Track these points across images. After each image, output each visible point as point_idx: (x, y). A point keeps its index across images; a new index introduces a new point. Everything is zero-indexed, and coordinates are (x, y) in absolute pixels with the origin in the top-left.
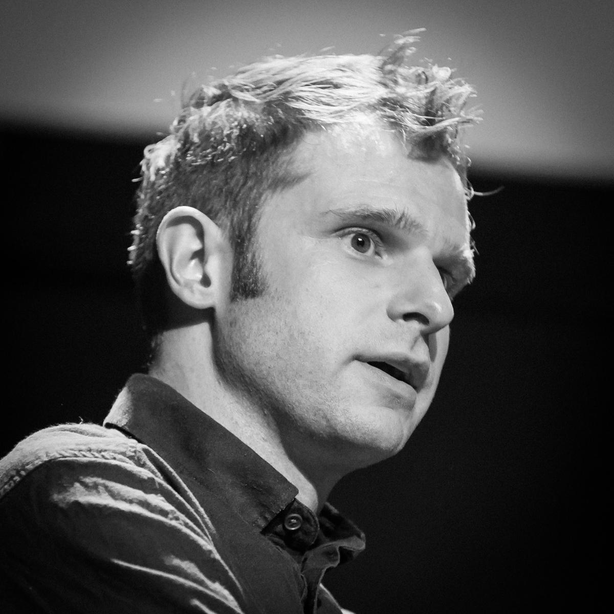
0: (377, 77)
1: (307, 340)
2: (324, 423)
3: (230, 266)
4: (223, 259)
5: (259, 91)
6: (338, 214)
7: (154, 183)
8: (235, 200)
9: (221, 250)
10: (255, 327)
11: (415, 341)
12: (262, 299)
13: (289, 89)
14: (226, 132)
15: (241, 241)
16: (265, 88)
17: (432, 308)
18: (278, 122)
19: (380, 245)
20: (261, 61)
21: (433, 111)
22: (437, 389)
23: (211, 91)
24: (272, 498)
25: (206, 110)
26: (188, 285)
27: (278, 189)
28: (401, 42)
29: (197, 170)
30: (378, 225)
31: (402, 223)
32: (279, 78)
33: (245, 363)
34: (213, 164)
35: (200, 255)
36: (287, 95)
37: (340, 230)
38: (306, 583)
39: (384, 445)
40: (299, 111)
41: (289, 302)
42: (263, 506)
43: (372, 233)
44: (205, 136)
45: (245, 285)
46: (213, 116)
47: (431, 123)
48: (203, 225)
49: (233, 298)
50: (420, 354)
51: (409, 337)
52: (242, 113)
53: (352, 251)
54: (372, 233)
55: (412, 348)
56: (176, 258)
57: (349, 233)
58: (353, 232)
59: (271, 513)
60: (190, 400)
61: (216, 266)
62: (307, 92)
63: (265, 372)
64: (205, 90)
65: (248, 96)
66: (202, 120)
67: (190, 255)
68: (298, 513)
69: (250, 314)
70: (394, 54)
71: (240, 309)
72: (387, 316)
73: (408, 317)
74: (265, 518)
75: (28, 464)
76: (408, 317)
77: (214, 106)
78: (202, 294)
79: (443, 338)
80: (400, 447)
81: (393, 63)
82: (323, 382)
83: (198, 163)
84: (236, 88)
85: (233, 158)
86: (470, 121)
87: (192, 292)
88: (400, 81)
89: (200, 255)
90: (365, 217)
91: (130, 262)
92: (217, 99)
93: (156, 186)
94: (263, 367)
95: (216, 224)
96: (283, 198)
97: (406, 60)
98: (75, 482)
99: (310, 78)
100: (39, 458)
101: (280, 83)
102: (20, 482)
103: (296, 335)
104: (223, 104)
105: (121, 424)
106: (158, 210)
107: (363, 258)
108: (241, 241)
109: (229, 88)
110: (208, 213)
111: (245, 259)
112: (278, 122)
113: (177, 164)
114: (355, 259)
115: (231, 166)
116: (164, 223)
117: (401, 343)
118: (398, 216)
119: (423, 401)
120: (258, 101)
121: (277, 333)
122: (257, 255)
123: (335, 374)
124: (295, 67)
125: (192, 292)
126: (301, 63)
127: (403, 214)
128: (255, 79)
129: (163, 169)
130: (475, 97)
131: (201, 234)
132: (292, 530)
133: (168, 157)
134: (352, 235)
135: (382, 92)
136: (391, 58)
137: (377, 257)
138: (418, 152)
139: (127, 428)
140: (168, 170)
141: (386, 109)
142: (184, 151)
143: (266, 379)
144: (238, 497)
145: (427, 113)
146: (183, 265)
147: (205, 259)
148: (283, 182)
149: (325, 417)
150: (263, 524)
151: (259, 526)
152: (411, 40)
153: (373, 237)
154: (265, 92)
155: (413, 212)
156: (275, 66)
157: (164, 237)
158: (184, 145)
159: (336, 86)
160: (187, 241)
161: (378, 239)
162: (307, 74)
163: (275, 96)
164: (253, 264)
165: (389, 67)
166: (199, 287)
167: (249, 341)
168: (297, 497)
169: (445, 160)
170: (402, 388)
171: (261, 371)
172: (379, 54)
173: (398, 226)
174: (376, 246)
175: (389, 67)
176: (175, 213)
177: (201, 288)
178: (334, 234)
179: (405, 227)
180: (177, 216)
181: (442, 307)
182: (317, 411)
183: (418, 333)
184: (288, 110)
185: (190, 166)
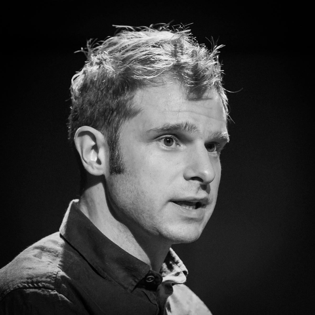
1: (145, 196)
6: (155, 131)
9: (104, 145)
10: (121, 189)
11: (199, 189)
12: (124, 174)
15: (112, 145)
17: (203, 174)
19: (178, 141)
26: (91, 164)
27: (126, 118)
30: (174, 132)
31: (187, 128)
35: (95, 148)
37: (157, 138)
38: (158, 308)
41: (136, 177)
42: (135, 276)
43: (173, 136)
45: (116, 167)
48: (95, 135)
49: (111, 173)
50: (202, 195)
51: (195, 188)
54: (173, 136)
55: (197, 192)
56: (84, 150)
57: (162, 139)
58: (163, 138)
59: (138, 279)
60: (96, 226)
68: (152, 275)
72: (183, 178)
73: (194, 178)
74: (135, 281)
76: (194, 178)
78: (98, 168)
87: (93, 168)
90: (168, 130)
96: (129, 123)
103: (140, 193)
107: (170, 149)
108: (112, 145)
114: (166, 151)
116: (77, 133)
117: (192, 191)
118: (184, 125)
119: (208, 211)
121: (131, 192)
123: (160, 211)
127: (186, 124)
130: (220, 53)
131: (94, 138)
132: (151, 282)
134: (163, 139)
137: (178, 146)
138: (192, 95)
143: (129, 213)
146: (88, 152)
149: (158, 231)
150: (135, 284)
151: (133, 285)
155: (191, 121)
160: (89, 142)
161: (177, 139)
164: (118, 155)
167: (120, 195)
171: (126, 209)
173: (185, 130)
174: (176, 141)
176: (79, 130)
177: (97, 165)
178: (155, 140)
179: (189, 130)
180: (79, 132)
183: (199, 186)
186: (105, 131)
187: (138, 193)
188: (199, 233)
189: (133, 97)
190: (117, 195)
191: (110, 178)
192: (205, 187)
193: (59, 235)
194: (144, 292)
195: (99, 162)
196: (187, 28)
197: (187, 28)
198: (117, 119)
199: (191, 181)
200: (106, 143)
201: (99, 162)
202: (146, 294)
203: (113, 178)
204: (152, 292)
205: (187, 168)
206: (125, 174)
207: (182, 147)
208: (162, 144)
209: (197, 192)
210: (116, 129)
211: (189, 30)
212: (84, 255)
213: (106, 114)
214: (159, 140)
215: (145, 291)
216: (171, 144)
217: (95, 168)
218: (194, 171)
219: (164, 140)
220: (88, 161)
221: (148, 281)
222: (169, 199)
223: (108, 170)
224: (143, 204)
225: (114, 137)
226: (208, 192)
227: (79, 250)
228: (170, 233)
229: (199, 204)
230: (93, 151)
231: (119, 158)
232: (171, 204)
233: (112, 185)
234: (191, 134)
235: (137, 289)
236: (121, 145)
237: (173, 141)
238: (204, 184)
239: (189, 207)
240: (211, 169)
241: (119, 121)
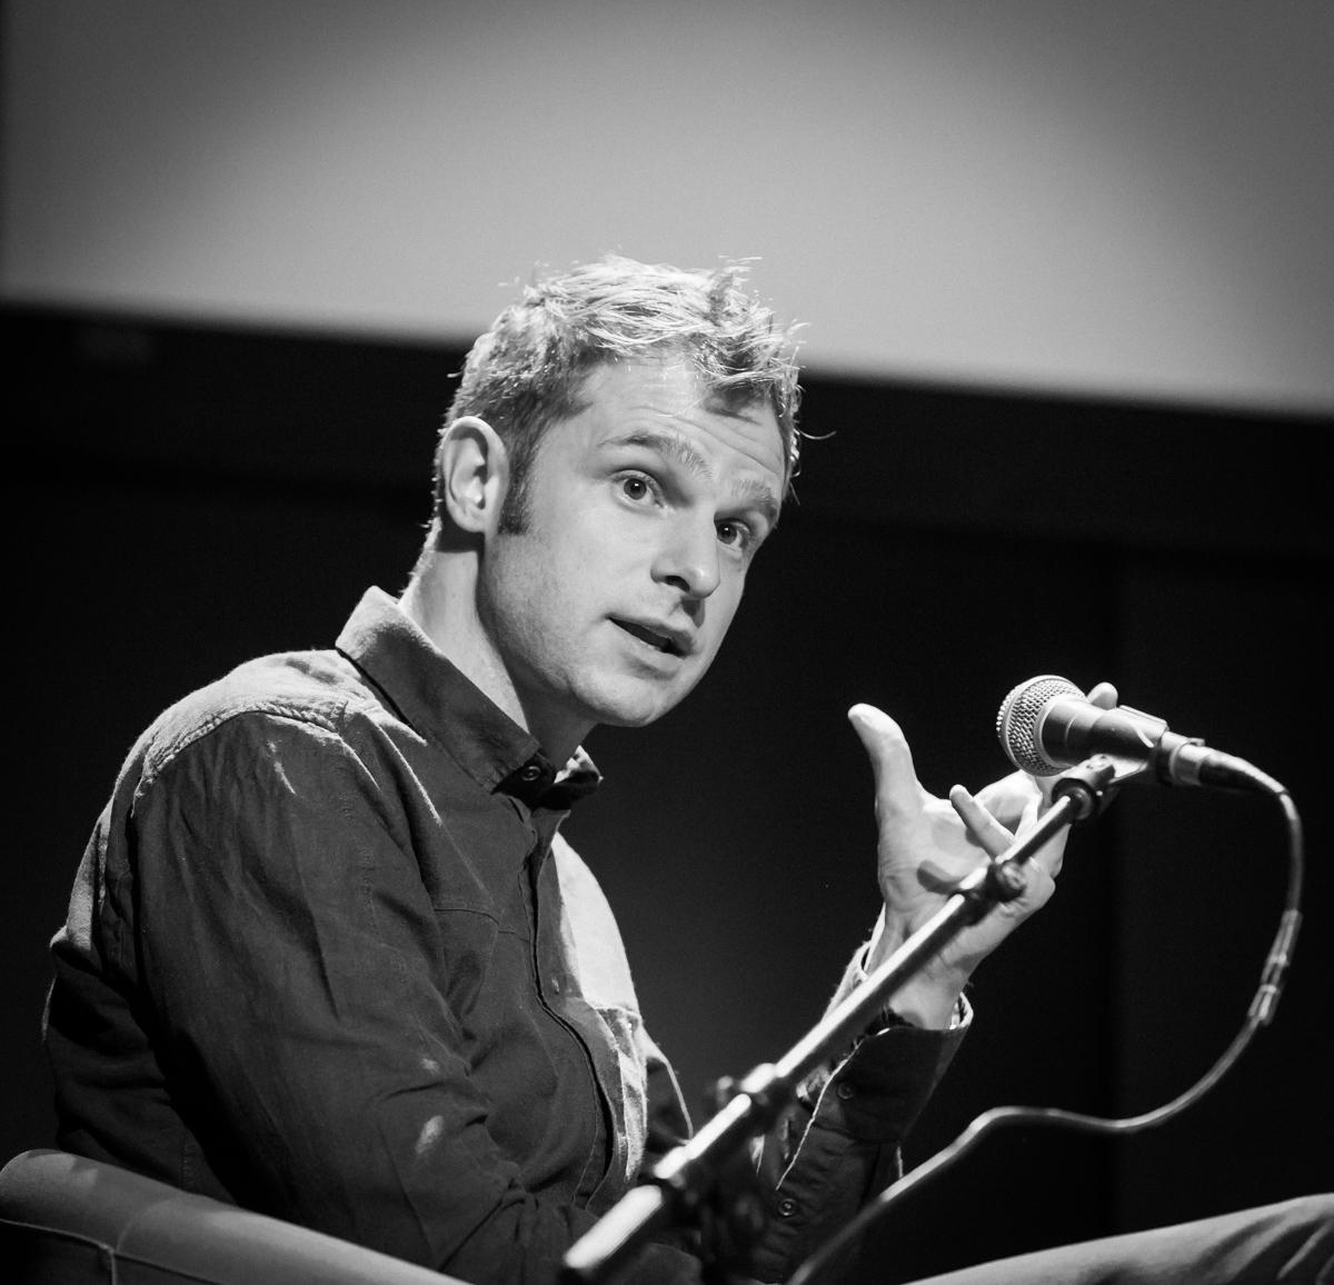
2: (564, 682)
4: (502, 481)
10: (513, 567)
13: (596, 311)
15: (519, 468)
17: (693, 574)
22: (716, 657)
26: (462, 503)
32: (595, 294)
33: (498, 602)
42: (501, 761)
43: (650, 483)
45: (512, 520)
49: (500, 530)
50: (681, 622)
53: (625, 498)
55: (671, 614)
57: (623, 478)
59: (507, 768)
67: (473, 469)
74: (501, 774)
75: (224, 712)
80: (649, 720)
82: (569, 640)
86: (665, 446)
87: (464, 512)
89: (482, 473)
94: (514, 612)
100: (235, 707)
102: (213, 731)
103: (549, 584)
105: (355, 657)
114: (626, 508)
117: (659, 607)
119: (689, 672)
123: (584, 633)
128: (574, 290)
131: (484, 449)
137: (657, 506)
138: (718, 402)
139: (359, 662)
144: (472, 750)
149: (566, 678)
151: (493, 781)
152: (742, 269)
159: (648, 313)
160: (472, 456)
164: (524, 494)
167: (506, 580)
170: (654, 657)
171: (511, 614)
177: (476, 510)
182: (560, 670)
183: (679, 600)
186: (510, 440)
187: (545, 584)
189: (588, 376)
192: (692, 605)
196: (1310, 1244)
197: (1310, 1244)
198: (541, 418)
199: (664, 585)
200: (507, 465)
201: (482, 505)
202: (514, 806)
205: (664, 555)
206: (529, 535)
207: (667, 510)
209: (671, 614)
210: (533, 441)
211: (747, 269)
213: (522, 403)
214: (617, 480)
216: (638, 495)
217: (469, 513)
218: (676, 563)
219: (626, 484)
220: (458, 495)
221: (526, 779)
222: (605, 610)
224: (549, 609)
225: (525, 454)
226: (698, 623)
228: (592, 686)
229: (673, 645)
230: (476, 480)
231: (525, 500)
232: (609, 624)
233: (496, 557)
236: (535, 473)
238: (693, 599)
240: (722, 578)
241: (545, 422)
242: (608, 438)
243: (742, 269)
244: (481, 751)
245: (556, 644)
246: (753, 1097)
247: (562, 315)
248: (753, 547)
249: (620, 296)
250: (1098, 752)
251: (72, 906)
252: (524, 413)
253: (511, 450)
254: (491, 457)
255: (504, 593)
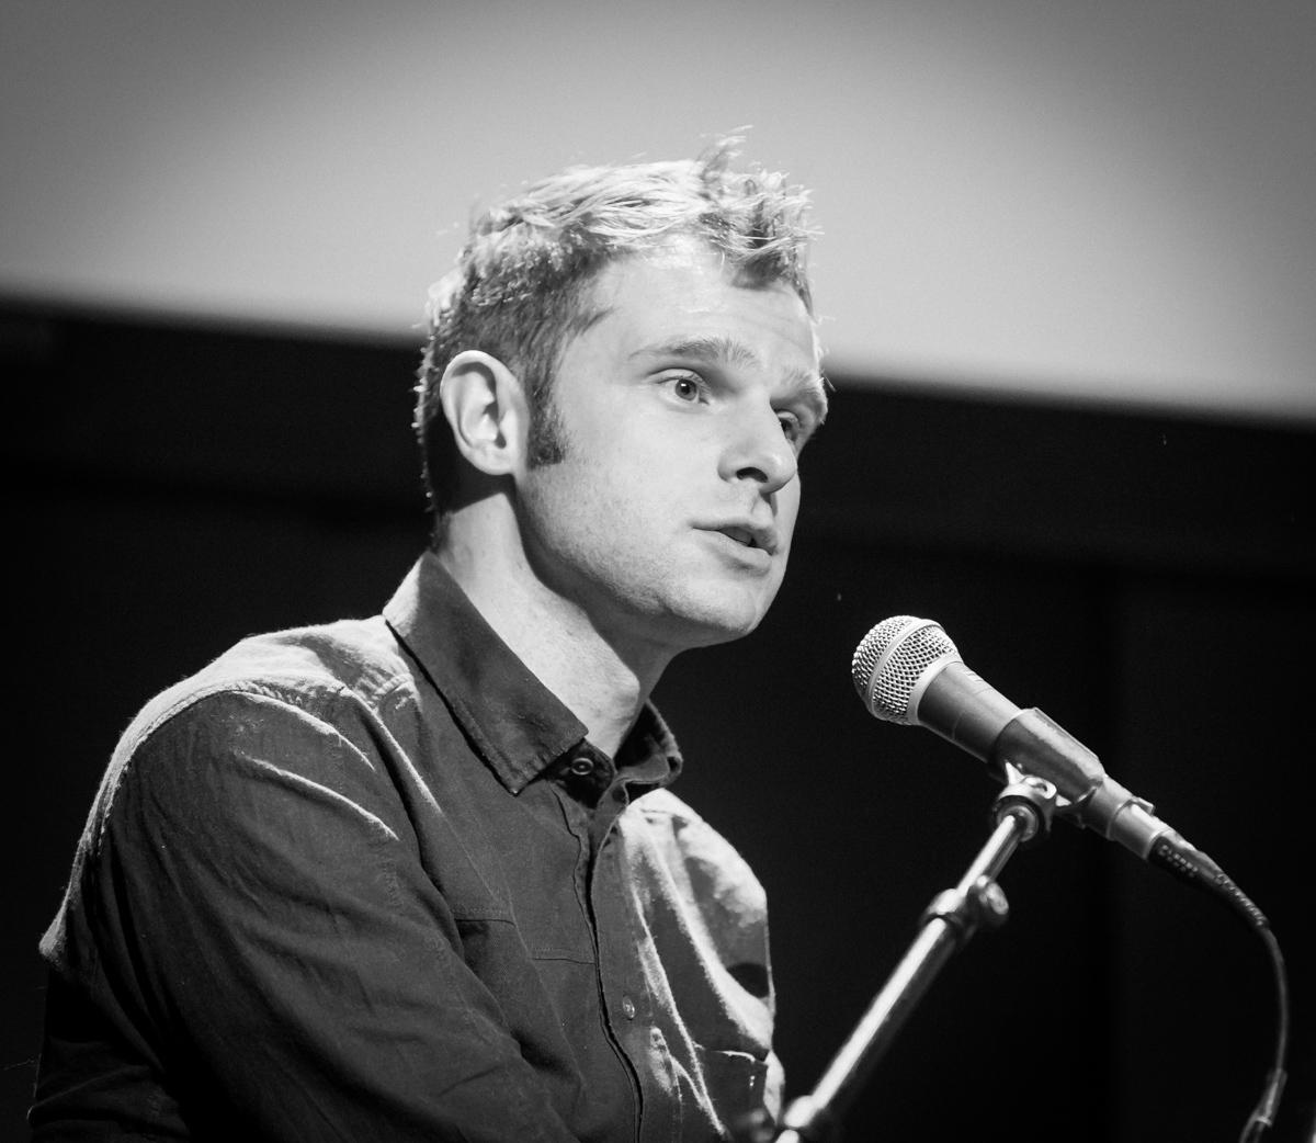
0: (697, 187)
2: (655, 603)
3: (527, 421)
5: (553, 214)
7: (438, 329)
8: (529, 347)
10: (559, 497)
11: (755, 502)
14: (518, 265)
15: (538, 393)
16: (562, 210)
18: (577, 251)
20: (562, 174)
21: (762, 230)
23: (501, 215)
24: (553, 737)
25: (496, 236)
26: (480, 446)
28: (723, 143)
29: (487, 311)
32: (578, 195)
34: (501, 306)
36: (587, 218)
39: (730, 624)
40: (604, 238)
43: (698, 377)
44: (494, 269)
45: (544, 449)
46: (504, 244)
47: (759, 244)
49: (532, 463)
50: (761, 517)
52: (537, 241)
54: (698, 377)
58: (674, 379)
59: (550, 754)
61: (512, 425)
62: (605, 211)
63: (572, 552)
64: (492, 214)
65: (540, 220)
66: (491, 252)
67: (482, 410)
69: (553, 483)
70: (716, 158)
71: (541, 477)
73: (744, 473)
74: (543, 760)
76: (744, 473)
77: (506, 230)
78: (498, 457)
79: (790, 497)
81: (716, 168)
83: (486, 303)
84: (527, 210)
85: (525, 296)
88: (727, 190)
89: (493, 410)
91: (415, 425)
92: (511, 222)
93: (441, 331)
94: (570, 546)
95: (512, 372)
97: (730, 165)
98: (41, 956)
99: (616, 194)
101: (579, 202)
103: (610, 503)
104: (514, 229)
106: (441, 360)
108: (538, 393)
109: (521, 210)
110: (499, 358)
111: (544, 415)
112: (577, 251)
113: (463, 305)
114: (683, 411)
115: (524, 304)
117: (742, 504)
119: (778, 567)
120: (552, 225)
122: (558, 407)
124: (597, 182)
125: (485, 453)
126: (609, 174)
128: (549, 198)
129: (448, 311)
131: (492, 384)
133: (454, 295)
135: (703, 207)
136: (711, 163)
137: (703, 405)
138: (745, 279)
140: (452, 312)
141: (707, 227)
142: (470, 289)
145: (754, 233)
147: (500, 415)
148: (586, 322)
149: (656, 597)
150: (540, 766)
151: (534, 768)
152: (735, 140)
153: (701, 384)
154: (562, 214)
156: (579, 177)
157: (449, 389)
158: (470, 281)
159: (647, 203)
160: (477, 392)
162: (614, 189)
163: (572, 219)
165: (711, 174)
166: (492, 448)
167: (553, 515)
168: (586, 737)
169: (779, 282)
171: (568, 550)
172: (698, 160)
175: (711, 174)
178: (644, 381)
181: (782, 457)
183: (756, 493)
184: (589, 236)
185: (477, 306)
187: (605, 505)
188: (754, 614)
190: (547, 515)
191: (531, 479)
193: (384, 622)
194: (558, 799)
195: (501, 442)
201: (501, 442)
202: (561, 804)
203: (538, 477)
204: (578, 805)
208: (669, 394)
212: (431, 669)
215: (562, 795)
219: (678, 386)
223: (523, 460)
227: (420, 657)
233: (535, 495)
234: (734, 371)
235: (543, 784)
237: (695, 391)
239: (481, 740)
242: (641, 347)
243: (735, 140)
244: (521, 733)
245: (635, 565)
246: (800, 1131)
247: (547, 224)
248: (801, 441)
249: (610, 190)
250: (786, 1084)
251: (389, 778)
252: (530, 336)
253: (522, 378)
254: (501, 389)
255: (555, 530)
